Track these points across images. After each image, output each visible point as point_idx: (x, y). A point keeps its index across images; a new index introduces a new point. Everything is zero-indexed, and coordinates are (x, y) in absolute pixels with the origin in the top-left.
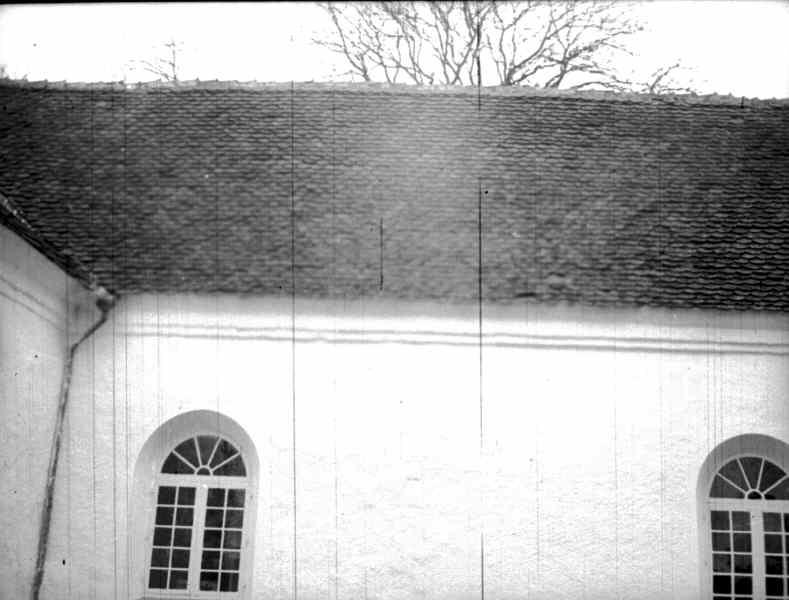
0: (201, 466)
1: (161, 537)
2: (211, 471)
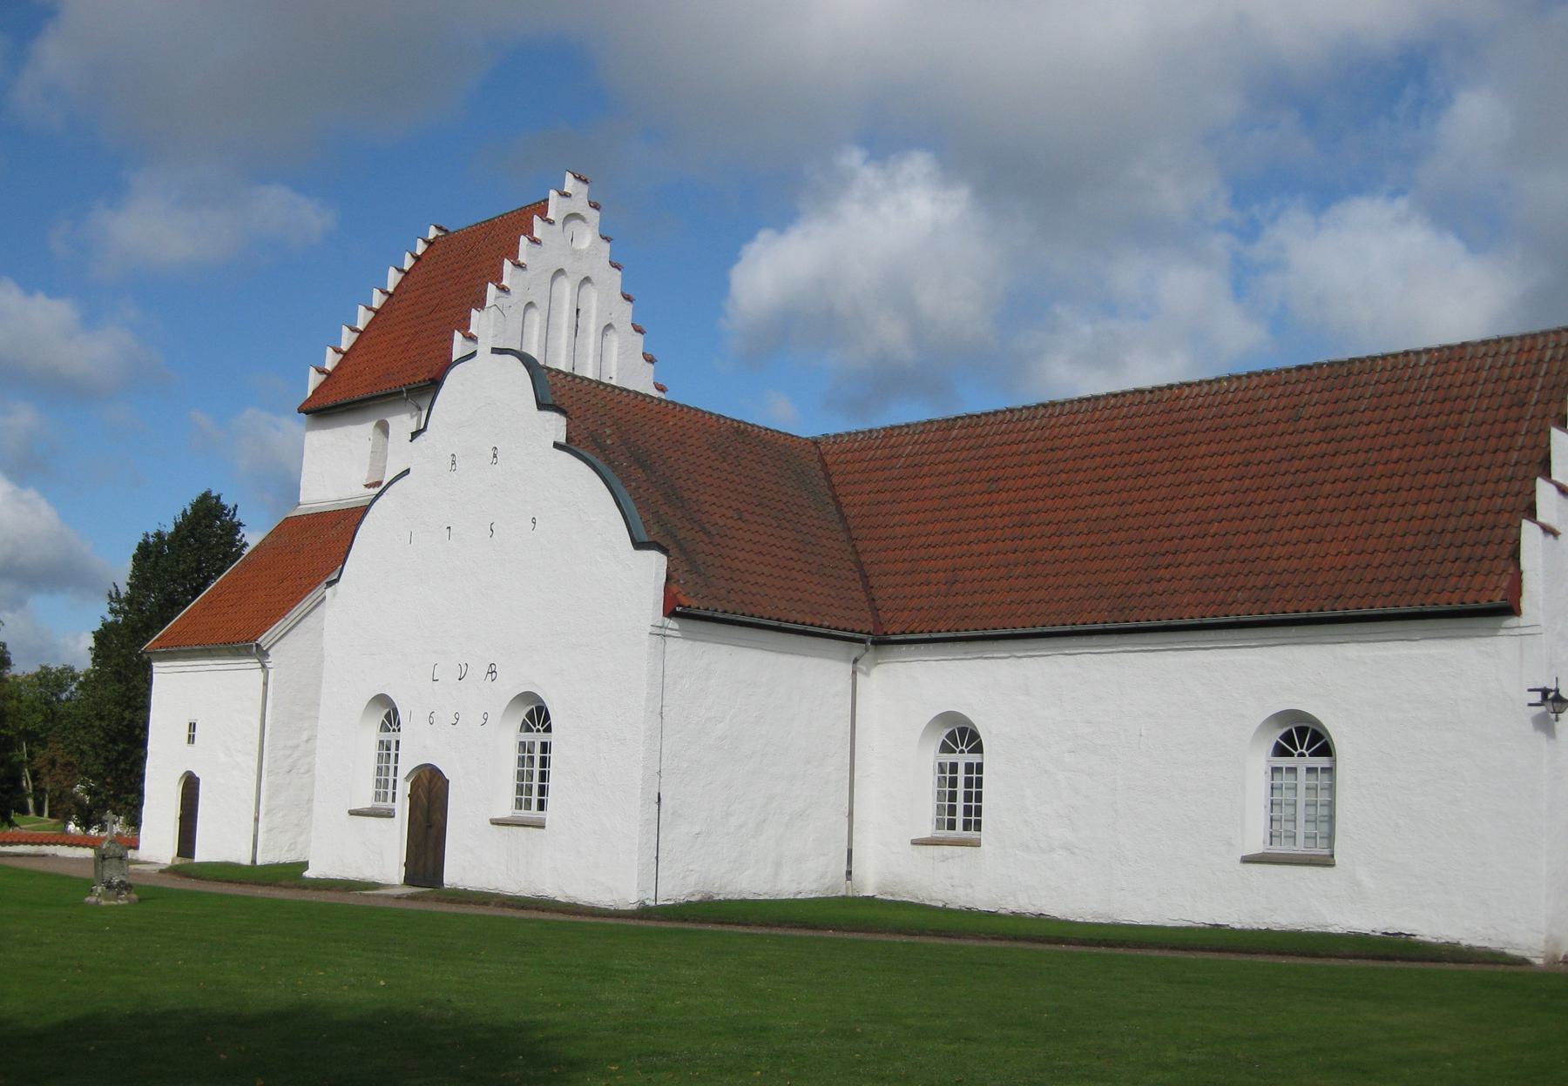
2: (966, 750)
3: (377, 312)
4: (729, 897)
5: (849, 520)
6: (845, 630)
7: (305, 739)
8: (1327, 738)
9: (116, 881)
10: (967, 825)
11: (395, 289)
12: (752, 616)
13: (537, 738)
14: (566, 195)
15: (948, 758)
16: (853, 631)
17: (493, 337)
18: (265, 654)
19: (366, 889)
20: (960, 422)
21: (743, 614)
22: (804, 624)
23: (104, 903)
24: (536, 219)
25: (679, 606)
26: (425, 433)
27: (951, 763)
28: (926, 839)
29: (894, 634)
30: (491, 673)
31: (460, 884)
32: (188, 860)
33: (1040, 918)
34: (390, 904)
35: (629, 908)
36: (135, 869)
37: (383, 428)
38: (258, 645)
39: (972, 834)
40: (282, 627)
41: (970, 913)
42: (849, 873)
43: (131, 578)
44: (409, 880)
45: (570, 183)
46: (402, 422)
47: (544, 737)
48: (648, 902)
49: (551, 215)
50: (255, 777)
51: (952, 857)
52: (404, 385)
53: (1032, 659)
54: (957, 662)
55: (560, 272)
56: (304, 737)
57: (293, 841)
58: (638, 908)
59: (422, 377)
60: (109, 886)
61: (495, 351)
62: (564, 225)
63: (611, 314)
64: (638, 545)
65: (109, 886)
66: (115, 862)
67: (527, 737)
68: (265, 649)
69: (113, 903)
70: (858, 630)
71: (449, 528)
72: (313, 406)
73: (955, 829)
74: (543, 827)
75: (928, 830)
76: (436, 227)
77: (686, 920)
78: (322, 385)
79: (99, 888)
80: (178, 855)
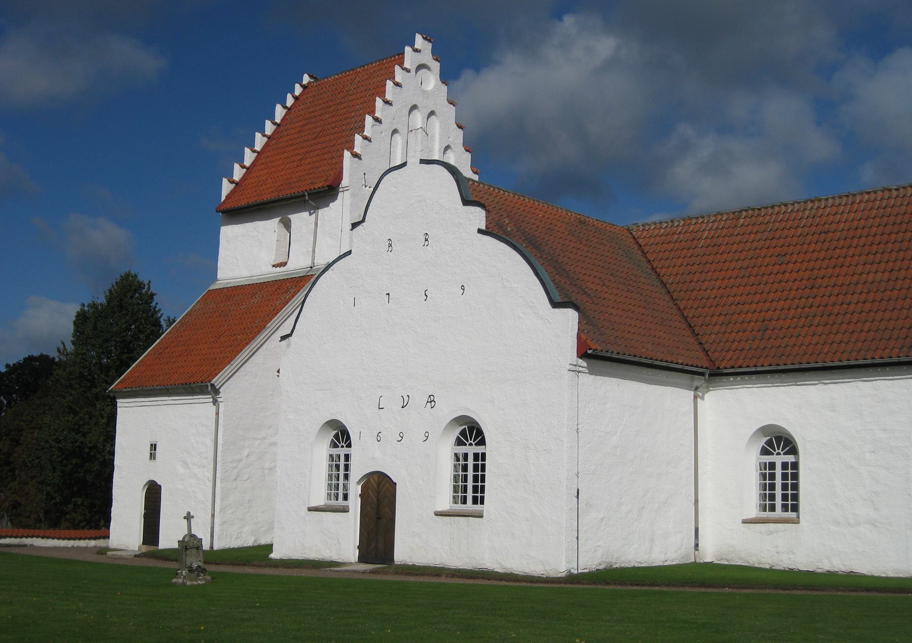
0: (777, 451)
1: (795, 487)
2: (782, 453)
3: (269, 138)
4: (623, 565)
5: (668, 286)
6: (692, 366)
7: (246, 455)
8: (794, 443)
9: (195, 566)
10: (475, 501)
11: (282, 121)
12: (635, 356)
13: (342, 451)
14: (417, 51)
15: (768, 459)
16: (697, 367)
17: (420, 151)
18: (217, 392)
19: (331, 566)
20: (744, 214)
21: (630, 355)
22: (667, 361)
23: (188, 583)
24: (397, 68)
25: (590, 349)
26: (363, 224)
27: (769, 463)
28: (752, 519)
29: (726, 368)
30: (431, 402)
31: (408, 561)
32: (152, 548)
33: (851, 575)
34: (357, 576)
35: (560, 575)
36: (112, 555)
37: (287, 225)
38: (212, 385)
39: (478, 507)
40: (230, 370)
41: (831, 574)
42: (697, 545)
43: (73, 337)
44: (363, 558)
45: (419, 41)
46: (301, 220)
47: (345, 450)
48: (572, 571)
49: (407, 65)
50: (210, 484)
51: (776, 532)
52: (306, 190)
53: (836, 385)
54: (775, 388)
55: (414, 107)
56: (246, 453)
57: (239, 531)
58: (566, 575)
59: (320, 184)
60: (191, 570)
61: (423, 161)
62: (416, 72)
63: (449, 138)
64: (555, 304)
65: (191, 570)
66: (194, 551)
67: (335, 451)
68: (217, 387)
69: (195, 583)
70: (700, 366)
71: (389, 294)
72: (228, 206)
73: (775, 511)
74: (481, 517)
75: (753, 511)
76: (309, 75)
77: (608, 584)
78: (232, 192)
79: (184, 572)
80: (143, 544)
